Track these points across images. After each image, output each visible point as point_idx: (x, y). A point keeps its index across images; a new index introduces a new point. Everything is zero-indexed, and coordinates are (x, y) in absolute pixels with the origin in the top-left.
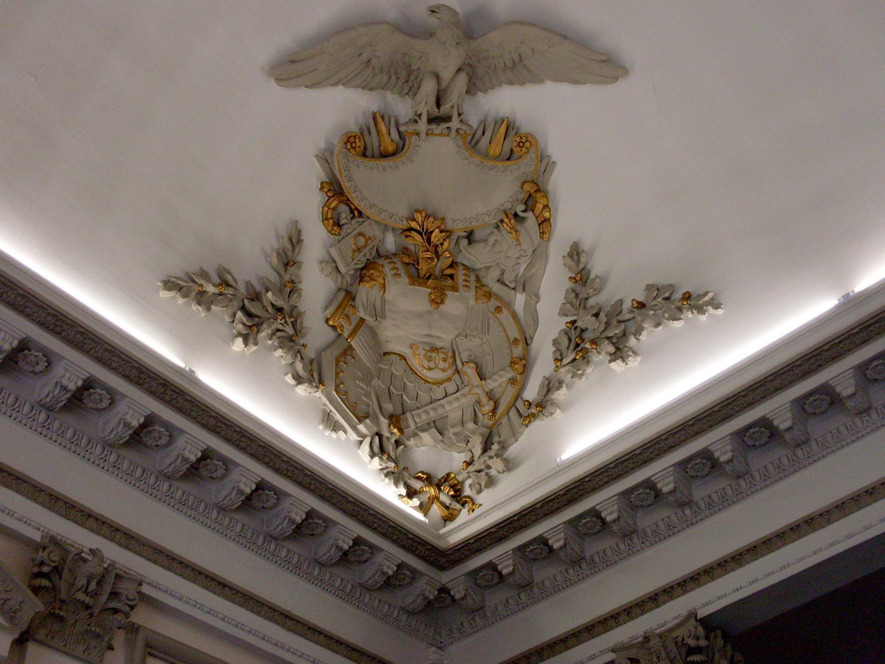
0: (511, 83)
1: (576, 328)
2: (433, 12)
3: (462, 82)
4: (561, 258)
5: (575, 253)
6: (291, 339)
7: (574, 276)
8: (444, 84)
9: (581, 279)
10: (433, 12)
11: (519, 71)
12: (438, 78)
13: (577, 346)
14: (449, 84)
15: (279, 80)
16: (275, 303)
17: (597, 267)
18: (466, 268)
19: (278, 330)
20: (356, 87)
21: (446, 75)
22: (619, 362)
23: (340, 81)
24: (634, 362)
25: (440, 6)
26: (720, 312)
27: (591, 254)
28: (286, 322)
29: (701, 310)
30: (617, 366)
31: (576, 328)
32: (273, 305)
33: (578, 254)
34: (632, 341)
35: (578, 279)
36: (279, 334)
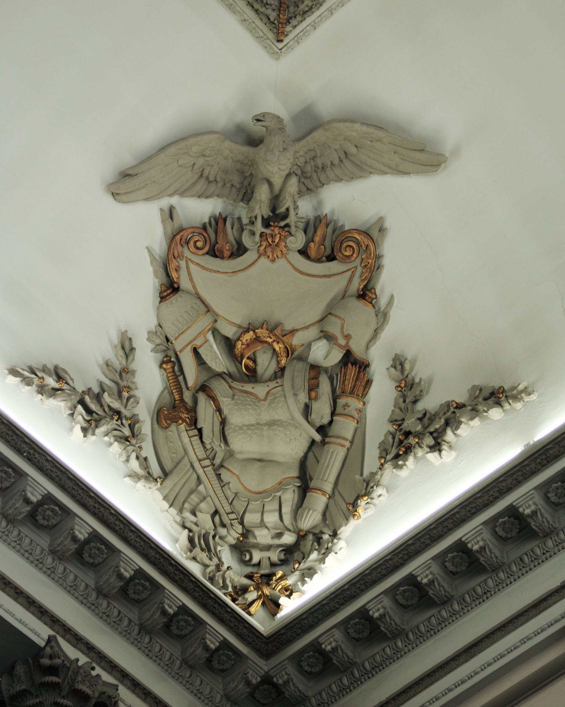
0: (339, 180)
1: (401, 430)
2: (258, 120)
3: (293, 185)
4: (386, 370)
5: (399, 363)
6: (127, 439)
7: (398, 384)
8: (277, 189)
9: (405, 386)
10: (258, 120)
11: (350, 164)
12: (270, 183)
13: (400, 447)
14: (281, 191)
15: (114, 195)
16: (111, 405)
17: (420, 373)
18: (327, 175)
19: (116, 430)
20: (192, 196)
21: (277, 181)
22: (436, 454)
23: (176, 191)
24: (448, 455)
25: (264, 115)
26: (534, 397)
27: (413, 363)
28: (122, 424)
29: (516, 398)
30: (432, 457)
31: (401, 430)
32: (109, 406)
33: (402, 364)
34: (449, 435)
35: (403, 385)
36: (116, 433)
